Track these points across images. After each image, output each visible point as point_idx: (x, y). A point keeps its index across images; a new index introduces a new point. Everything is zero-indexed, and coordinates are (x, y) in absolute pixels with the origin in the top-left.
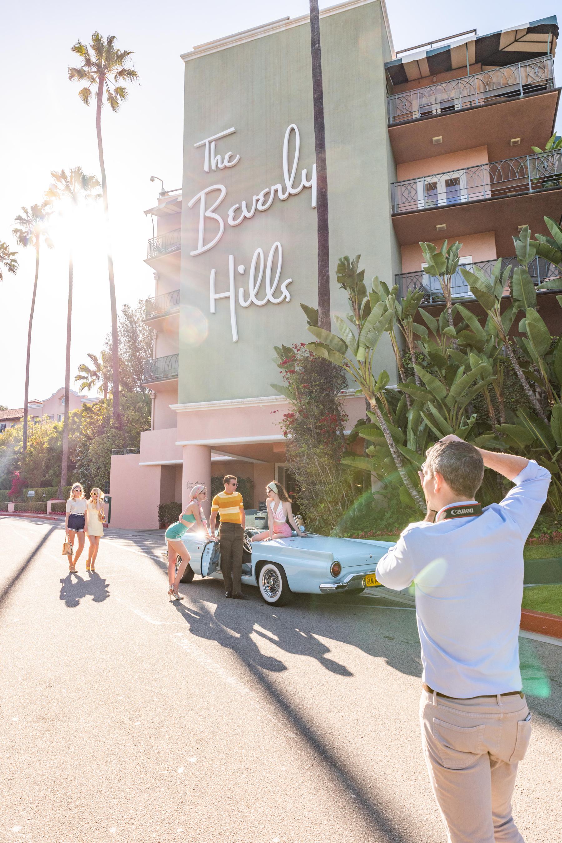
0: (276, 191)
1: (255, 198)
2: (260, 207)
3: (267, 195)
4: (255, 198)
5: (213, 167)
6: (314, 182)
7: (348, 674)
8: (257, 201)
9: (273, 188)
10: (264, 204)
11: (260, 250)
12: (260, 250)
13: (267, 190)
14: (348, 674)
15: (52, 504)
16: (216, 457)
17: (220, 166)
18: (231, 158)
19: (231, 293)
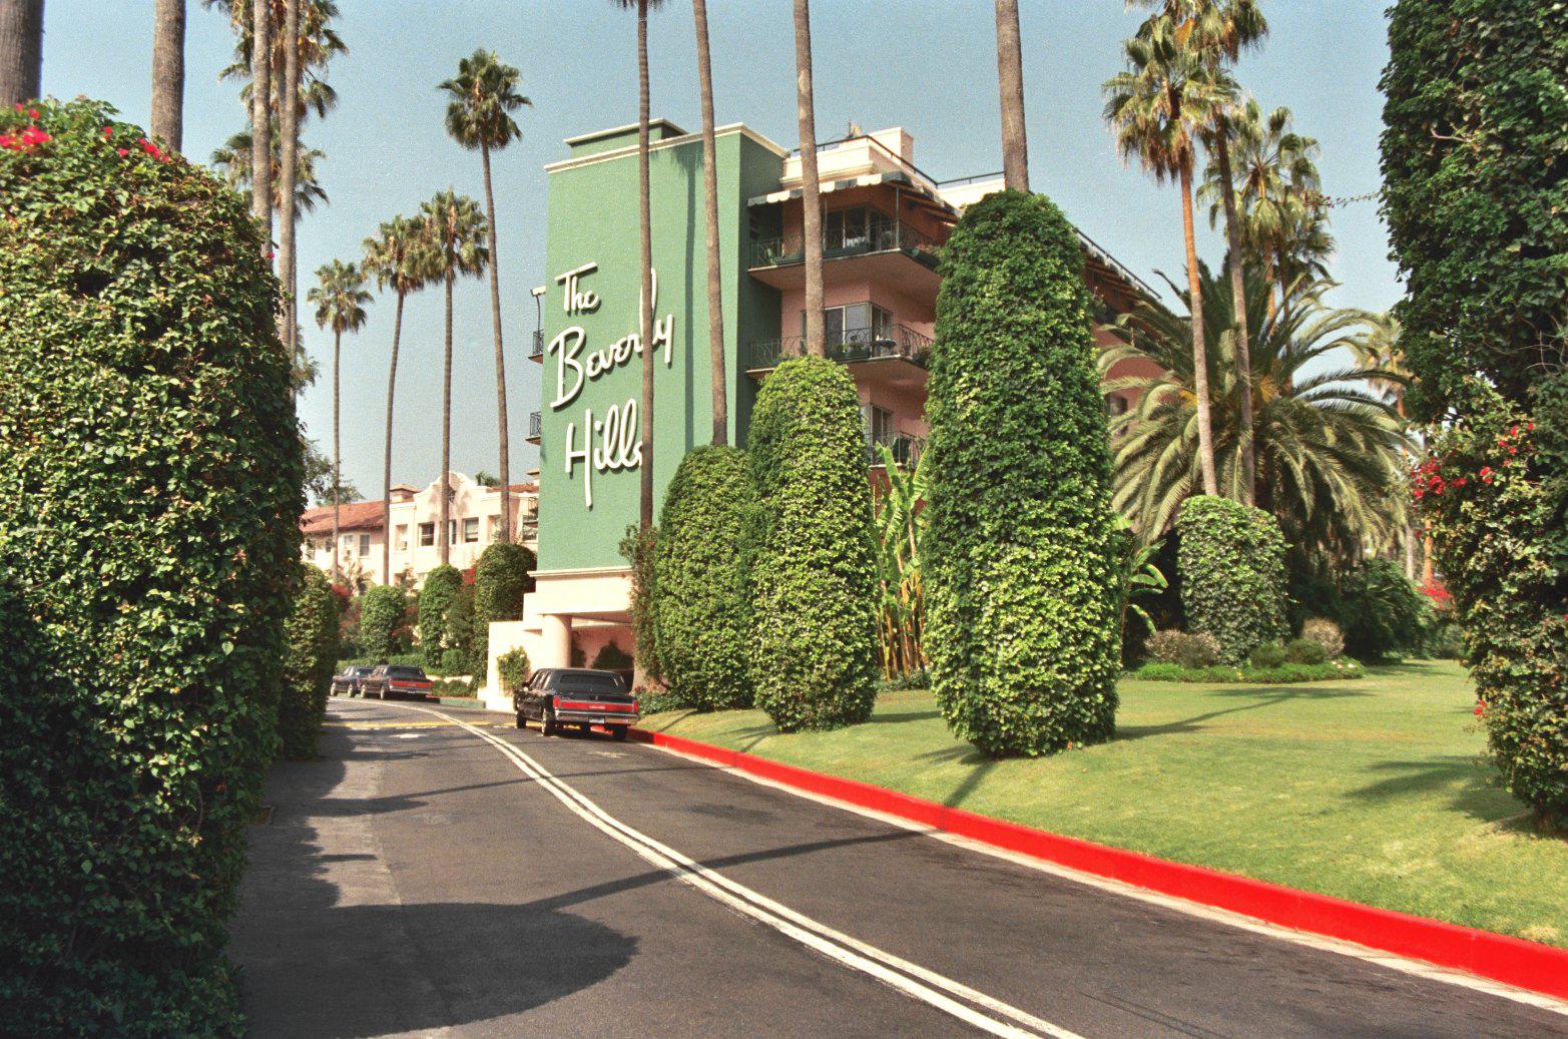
3: (624, 345)
4: (612, 347)
6: (667, 336)
10: (622, 354)
11: (615, 408)
12: (615, 408)
16: (576, 624)
18: (592, 298)
19: (586, 453)
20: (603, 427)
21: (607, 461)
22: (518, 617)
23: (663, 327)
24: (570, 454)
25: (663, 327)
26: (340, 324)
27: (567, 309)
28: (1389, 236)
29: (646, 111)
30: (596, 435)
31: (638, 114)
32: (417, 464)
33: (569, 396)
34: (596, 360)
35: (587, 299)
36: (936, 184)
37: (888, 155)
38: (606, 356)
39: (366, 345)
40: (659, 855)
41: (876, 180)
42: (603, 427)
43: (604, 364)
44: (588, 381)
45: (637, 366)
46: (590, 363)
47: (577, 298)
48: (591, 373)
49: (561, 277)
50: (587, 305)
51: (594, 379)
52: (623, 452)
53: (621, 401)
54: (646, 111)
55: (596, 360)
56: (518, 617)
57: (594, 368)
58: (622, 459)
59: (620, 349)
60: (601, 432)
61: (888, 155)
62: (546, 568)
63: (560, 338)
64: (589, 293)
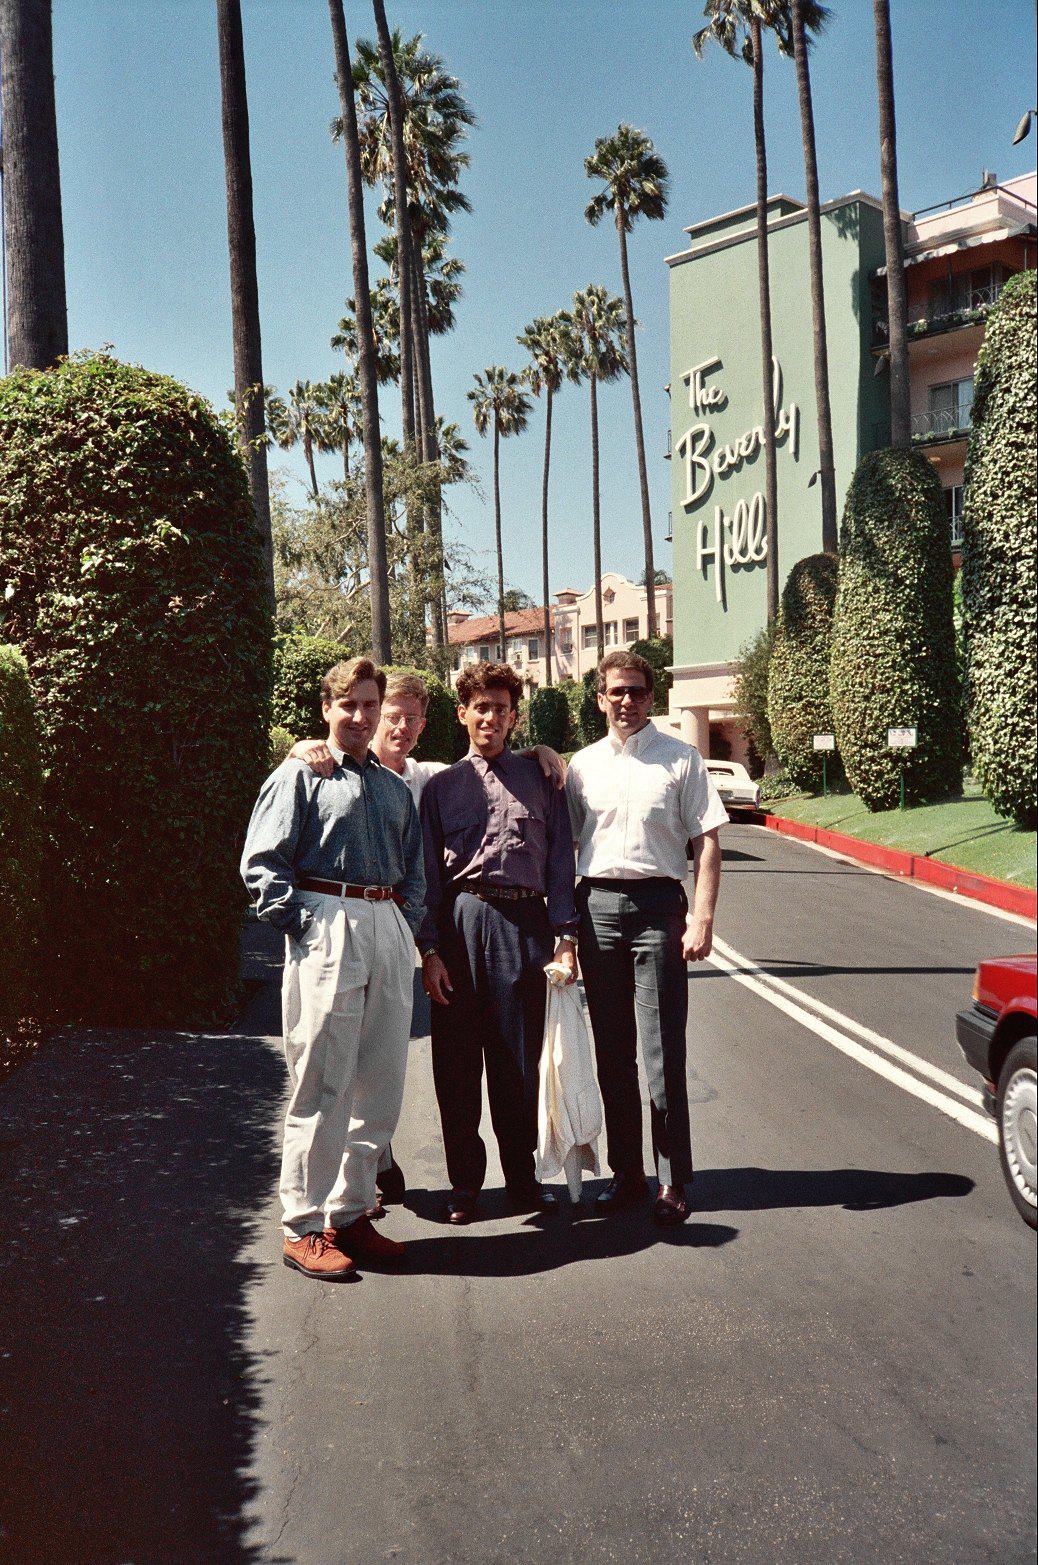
1: (737, 441)
2: (744, 453)
4: (737, 441)
5: (699, 404)
6: (791, 425)
8: (740, 444)
9: (754, 431)
14: (726, 609)
16: (713, 716)
17: (705, 403)
21: (737, 555)
22: (667, 713)
24: (701, 552)
27: (692, 405)
44: (717, 479)
48: (717, 470)
52: (751, 548)
55: (723, 458)
56: (667, 713)
57: (721, 465)
58: (752, 555)
59: (745, 443)
63: (687, 437)
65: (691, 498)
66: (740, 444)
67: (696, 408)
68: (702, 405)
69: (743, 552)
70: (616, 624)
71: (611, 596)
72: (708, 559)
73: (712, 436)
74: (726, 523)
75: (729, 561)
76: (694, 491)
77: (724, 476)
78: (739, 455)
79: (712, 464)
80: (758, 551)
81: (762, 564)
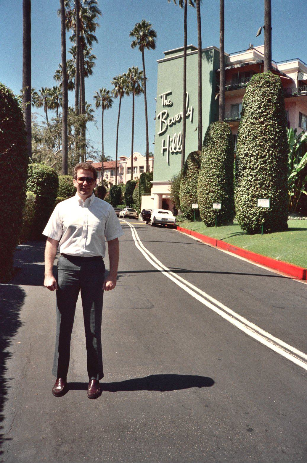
0: (181, 114)
2: (177, 120)
4: (175, 116)
5: (164, 104)
6: (191, 113)
7: (169, 165)
8: (176, 117)
12: (175, 134)
13: (178, 114)
14: (169, 165)
15: (152, 181)
16: (164, 197)
17: (166, 104)
18: (170, 102)
20: (172, 140)
23: (190, 111)
24: (163, 148)
25: (190, 111)
26: (104, 107)
27: (162, 105)
28: (8, 348)
29: (186, 45)
30: (171, 142)
31: (183, 43)
32: (124, 151)
33: (164, 130)
34: (171, 121)
35: (168, 102)
36: (276, 63)
37: (260, 54)
38: (174, 119)
39: (111, 113)
40: (158, 265)
41: (254, 62)
42: (172, 140)
43: (173, 121)
44: (169, 126)
45: (180, 125)
46: (169, 121)
47: (165, 101)
48: (169, 124)
49: (160, 95)
50: (168, 104)
51: (171, 126)
52: (178, 147)
53: (177, 131)
54: (186, 45)
55: (171, 121)
57: (170, 123)
58: (177, 150)
59: (177, 117)
60: (172, 141)
61: (260, 54)
62: (189, 44)
63: (161, 114)
64: (169, 100)
65: (161, 132)
66: (176, 117)
67: (164, 105)
68: (165, 105)
69: (175, 149)
70: (137, 167)
71: (136, 159)
72: (165, 150)
73: (168, 114)
74: (171, 140)
75: (171, 151)
76: (162, 130)
77: (171, 126)
78: (175, 120)
79: (167, 122)
80: (179, 149)
81: (180, 153)
